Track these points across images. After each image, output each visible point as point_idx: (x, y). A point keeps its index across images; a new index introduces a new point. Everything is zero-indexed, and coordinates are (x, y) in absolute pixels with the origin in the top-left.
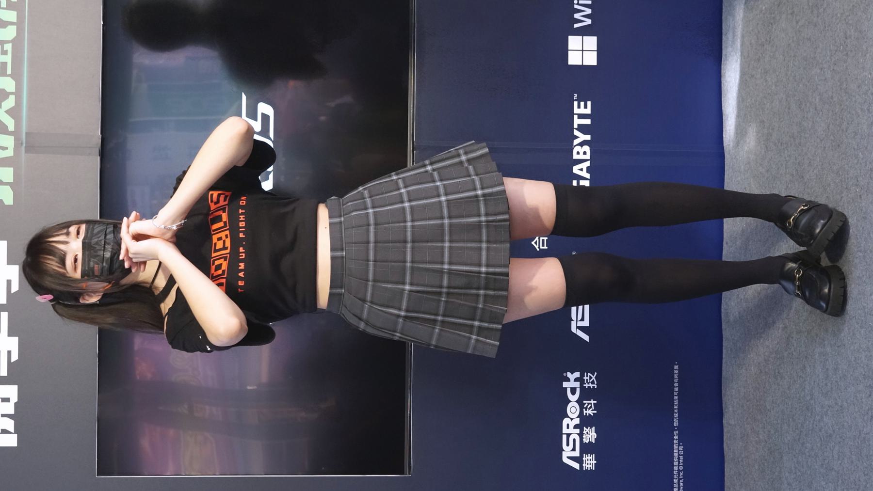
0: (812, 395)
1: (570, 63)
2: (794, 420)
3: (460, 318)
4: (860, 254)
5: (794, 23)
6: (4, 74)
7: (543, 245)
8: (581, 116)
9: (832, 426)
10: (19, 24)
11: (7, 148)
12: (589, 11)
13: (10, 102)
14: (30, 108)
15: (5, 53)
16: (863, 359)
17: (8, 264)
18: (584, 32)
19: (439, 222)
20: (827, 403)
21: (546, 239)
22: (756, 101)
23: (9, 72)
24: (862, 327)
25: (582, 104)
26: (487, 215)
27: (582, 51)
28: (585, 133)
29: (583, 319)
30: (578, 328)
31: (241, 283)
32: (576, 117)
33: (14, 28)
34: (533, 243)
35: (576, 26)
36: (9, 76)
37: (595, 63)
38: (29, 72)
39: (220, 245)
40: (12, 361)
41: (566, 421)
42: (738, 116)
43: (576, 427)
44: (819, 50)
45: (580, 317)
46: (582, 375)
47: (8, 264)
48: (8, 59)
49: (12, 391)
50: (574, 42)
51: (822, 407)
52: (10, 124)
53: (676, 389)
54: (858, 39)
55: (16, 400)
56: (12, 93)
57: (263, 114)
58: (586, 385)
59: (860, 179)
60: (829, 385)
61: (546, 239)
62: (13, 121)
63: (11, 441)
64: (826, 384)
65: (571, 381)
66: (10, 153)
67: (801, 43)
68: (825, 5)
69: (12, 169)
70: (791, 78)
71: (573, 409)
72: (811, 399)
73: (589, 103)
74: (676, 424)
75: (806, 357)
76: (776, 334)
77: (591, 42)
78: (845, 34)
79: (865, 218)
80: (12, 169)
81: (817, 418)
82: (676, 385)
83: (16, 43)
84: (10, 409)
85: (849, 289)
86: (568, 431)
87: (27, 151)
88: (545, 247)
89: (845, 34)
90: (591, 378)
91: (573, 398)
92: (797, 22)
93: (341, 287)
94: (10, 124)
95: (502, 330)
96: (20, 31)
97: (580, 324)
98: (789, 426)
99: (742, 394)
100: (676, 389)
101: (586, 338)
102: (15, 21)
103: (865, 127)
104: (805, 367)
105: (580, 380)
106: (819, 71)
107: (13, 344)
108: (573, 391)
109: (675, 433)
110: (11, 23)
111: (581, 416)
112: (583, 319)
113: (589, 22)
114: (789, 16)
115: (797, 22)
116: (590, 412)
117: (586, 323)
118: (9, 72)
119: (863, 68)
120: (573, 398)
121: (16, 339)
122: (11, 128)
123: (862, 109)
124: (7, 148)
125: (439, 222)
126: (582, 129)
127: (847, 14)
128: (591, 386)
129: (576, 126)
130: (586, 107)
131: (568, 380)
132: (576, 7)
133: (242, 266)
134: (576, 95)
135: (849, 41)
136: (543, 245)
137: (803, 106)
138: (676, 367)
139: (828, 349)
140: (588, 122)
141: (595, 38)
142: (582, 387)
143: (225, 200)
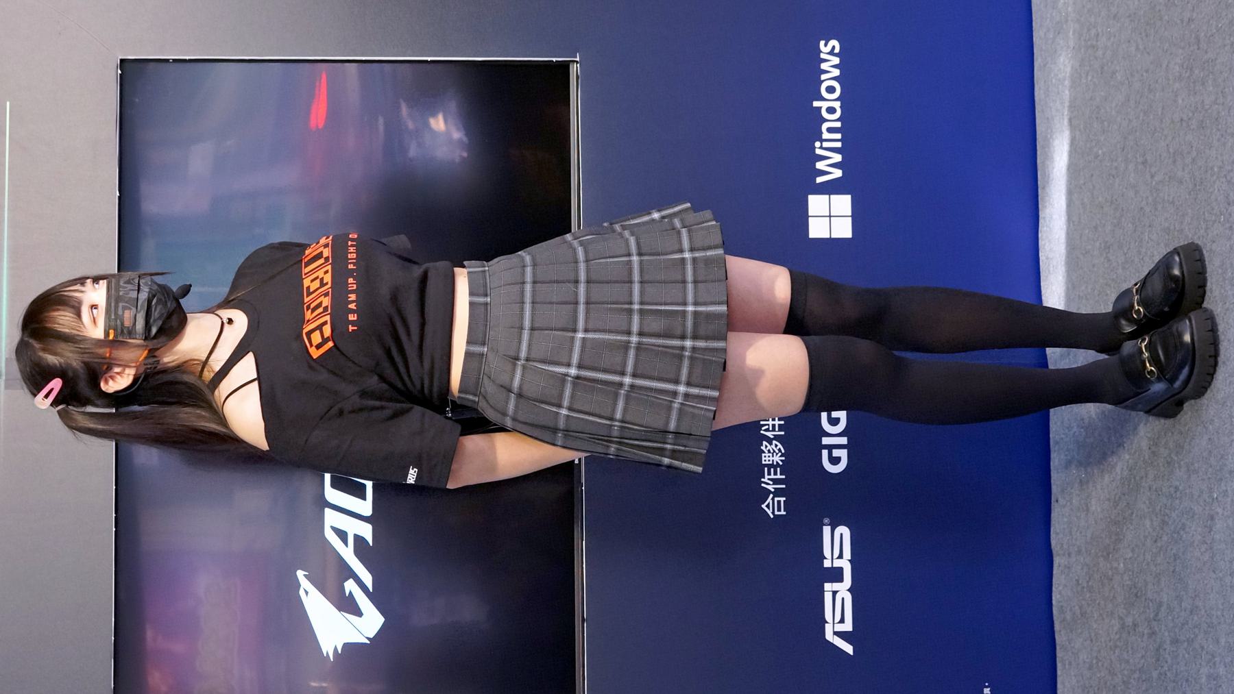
1: (811, 236)
5: (1148, 176)
7: (779, 510)
12: (838, 158)
18: (831, 188)
19: (625, 338)
21: (783, 499)
26: (692, 250)
29: (842, 621)
30: (836, 633)
31: (352, 317)
35: (819, 180)
39: (317, 284)
44: (1188, 219)
50: (816, 203)
57: (364, 498)
67: (1160, 207)
68: (1194, 154)
75: (1187, 681)
76: (1121, 463)
77: (843, 203)
78: (1227, 197)
85: (1221, 328)
92: (1152, 177)
101: (848, 649)
112: (842, 621)
113: (838, 173)
114: (1140, 167)
115: (1152, 177)
117: (848, 626)
125: (625, 338)
126: (836, 575)
132: (818, 152)
133: (353, 297)
136: (779, 510)
139: (1221, 670)
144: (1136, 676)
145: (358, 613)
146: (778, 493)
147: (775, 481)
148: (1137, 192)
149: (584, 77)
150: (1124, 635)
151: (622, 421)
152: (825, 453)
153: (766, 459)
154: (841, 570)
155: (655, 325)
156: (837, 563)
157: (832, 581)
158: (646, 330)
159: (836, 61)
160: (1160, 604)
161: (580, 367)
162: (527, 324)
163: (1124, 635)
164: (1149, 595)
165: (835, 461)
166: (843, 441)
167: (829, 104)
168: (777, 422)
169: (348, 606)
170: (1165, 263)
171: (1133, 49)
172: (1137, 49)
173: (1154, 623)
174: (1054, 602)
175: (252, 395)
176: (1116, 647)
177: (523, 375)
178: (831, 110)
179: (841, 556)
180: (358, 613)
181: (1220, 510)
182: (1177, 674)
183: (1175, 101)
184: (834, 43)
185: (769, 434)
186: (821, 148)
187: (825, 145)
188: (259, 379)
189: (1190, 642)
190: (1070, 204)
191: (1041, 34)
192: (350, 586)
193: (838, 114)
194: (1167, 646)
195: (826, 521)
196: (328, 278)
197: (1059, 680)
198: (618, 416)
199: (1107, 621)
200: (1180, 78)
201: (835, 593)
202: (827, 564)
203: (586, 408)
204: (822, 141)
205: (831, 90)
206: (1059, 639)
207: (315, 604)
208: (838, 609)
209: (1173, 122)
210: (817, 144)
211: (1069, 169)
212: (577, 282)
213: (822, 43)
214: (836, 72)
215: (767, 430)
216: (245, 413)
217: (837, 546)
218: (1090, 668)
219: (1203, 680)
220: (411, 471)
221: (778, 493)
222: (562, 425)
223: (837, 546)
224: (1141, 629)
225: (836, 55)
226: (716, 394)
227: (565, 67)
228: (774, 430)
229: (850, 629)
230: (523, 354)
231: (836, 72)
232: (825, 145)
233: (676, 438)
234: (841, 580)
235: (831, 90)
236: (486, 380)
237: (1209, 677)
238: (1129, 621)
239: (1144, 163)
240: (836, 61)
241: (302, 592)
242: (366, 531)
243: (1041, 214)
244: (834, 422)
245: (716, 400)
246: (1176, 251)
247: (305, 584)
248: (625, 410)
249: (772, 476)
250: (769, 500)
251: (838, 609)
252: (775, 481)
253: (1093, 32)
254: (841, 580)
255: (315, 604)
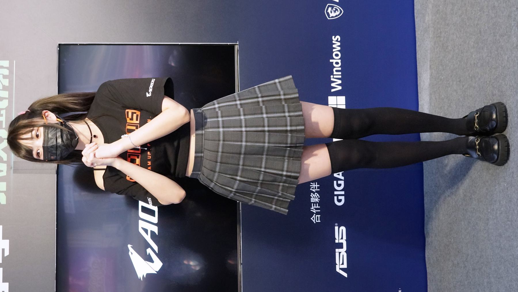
4: (509, 223)
5: (461, 87)
10: (10, 99)
11: (2, 171)
12: (340, 82)
15: (2, 115)
16: (514, 286)
18: (337, 94)
21: (319, 216)
24: (512, 267)
29: (343, 264)
30: (340, 269)
35: (333, 90)
36: (4, 129)
40: (5, 255)
45: (341, 263)
57: (154, 216)
59: (506, 178)
63: (4, 202)
66: (4, 174)
68: (479, 76)
69: (5, 183)
75: (479, 285)
80: (5, 183)
87: (14, 173)
88: (319, 221)
92: (463, 86)
93: (199, 171)
95: (297, 187)
96: (10, 102)
97: (342, 267)
101: (345, 275)
107: (6, 244)
110: (5, 98)
112: (343, 264)
113: (340, 88)
114: (458, 83)
115: (463, 86)
117: (345, 266)
121: (8, 284)
122: (5, 159)
124: (2, 171)
126: (340, 246)
127: (493, 81)
132: (332, 79)
143: (137, 120)
145: (152, 261)
146: (317, 213)
147: (316, 209)
149: (240, 50)
152: (336, 198)
153: (312, 200)
154: (342, 244)
156: (341, 241)
159: (339, 44)
160: (468, 255)
165: (339, 201)
166: (343, 193)
167: (336, 61)
168: (317, 186)
169: (149, 259)
171: (455, 37)
172: (457, 37)
174: (426, 256)
178: (337, 63)
179: (342, 238)
180: (152, 261)
181: (491, 216)
184: (338, 37)
185: (314, 190)
187: (335, 77)
191: (419, 33)
192: (149, 251)
195: (336, 224)
201: (340, 253)
202: (337, 241)
204: (333, 75)
205: (337, 55)
206: (429, 270)
207: (135, 258)
208: (341, 260)
210: (332, 76)
213: (333, 37)
214: (339, 48)
215: (313, 189)
217: (341, 234)
221: (317, 213)
223: (341, 234)
225: (339, 42)
226: (303, 127)
227: (233, 47)
228: (315, 189)
231: (339, 48)
232: (335, 77)
234: (342, 248)
235: (337, 55)
238: (456, 262)
241: (130, 254)
242: (155, 229)
244: (339, 185)
249: (315, 207)
250: (314, 216)
251: (341, 260)
252: (316, 209)
253: (439, 31)
254: (342, 248)
255: (135, 258)
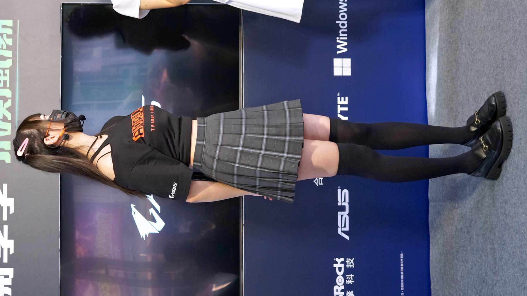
0: (486, 273)
1: (335, 75)
2: (475, 288)
3: (276, 151)
4: (515, 190)
6: (5, 87)
8: (342, 106)
9: (500, 292)
10: (14, 58)
11: (7, 130)
12: (346, 44)
13: (9, 103)
14: (20, 106)
15: (5, 75)
16: (518, 252)
17: (8, 197)
18: (343, 56)
20: (496, 278)
22: (447, 96)
23: (8, 86)
24: (517, 233)
25: (343, 98)
27: (342, 67)
28: (344, 116)
29: (345, 227)
30: (342, 231)
32: (339, 106)
33: (11, 60)
34: (314, 181)
35: (338, 52)
37: (350, 74)
38: (20, 86)
40: (10, 254)
41: (336, 287)
42: (437, 105)
43: (342, 291)
44: (486, 67)
45: (343, 225)
46: (345, 260)
47: (8, 197)
48: (7, 78)
49: (10, 272)
50: (337, 62)
51: (493, 281)
52: (9, 116)
53: (402, 268)
54: (510, 60)
55: (13, 277)
56: (9, 98)
58: (348, 266)
60: (497, 267)
61: (322, 179)
62: (10, 114)
64: (495, 267)
65: (339, 264)
67: (475, 62)
70: (469, 83)
71: (340, 280)
72: (486, 276)
73: (347, 98)
74: (402, 289)
77: (347, 62)
78: (503, 57)
79: (517, 168)
81: (490, 287)
82: (402, 265)
83: (12, 69)
84: (9, 282)
86: (337, 294)
88: (322, 184)
89: (503, 57)
90: (350, 261)
91: (340, 274)
92: (472, 50)
94: (9, 116)
96: (14, 62)
97: (344, 229)
98: (472, 291)
99: (443, 271)
100: (402, 268)
101: (347, 238)
102: (11, 56)
103: (516, 113)
104: (481, 256)
105: (344, 263)
106: (486, 79)
108: (340, 269)
109: (402, 289)
110: (9, 58)
111: (345, 284)
112: (345, 227)
113: (345, 50)
114: (467, 46)
115: (472, 50)
116: (350, 282)
117: (347, 229)
118: (8, 86)
119: (514, 78)
120: (340, 274)
122: (9, 118)
123: (514, 103)
124: (7, 130)
126: (343, 208)
127: (504, 45)
128: (351, 266)
129: (339, 112)
130: (345, 100)
131: (337, 263)
132: (338, 41)
133: (153, 120)
134: (339, 94)
135: (504, 61)
137: (477, 100)
138: (402, 255)
139: (496, 246)
140: (346, 109)
141: (350, 60)
142: (345, 267)
144: (462, 248)
145: (155, 221)
148: (466, 56)
150: (457, 233)
151: (261, 168)
154: (345, 206)
155: (274, 131)
156: (343, 204)
157: (341, 211)
158: (270, 133)
159: (346, 5)
161: (243, 147)
162: (221, 132)
163: (457, 233)
164: (468, 217)
170: (488, 101)
173: (469, 228)
175: (109, 157)
176: (454, 237)
177: (220, 151)
178: (343, 25)
179: (345, 201)
180: (155, 221)
182: (478, 248)
183: (482, 19)
186: (339, 40)
187: (341, 38)
188: (112, 152)
189: (484, 235)
190: (439, 62)
192: (152, 211)
193: (346, 26)
194: (474, 237)
195: (339, 187)
196: (143, 116)
197: (431, 251)
198: (259, 165)
199: (450, 227)
200: (484, 10)
201: (342, 216)
202: (339, 204)
203: (246, 163)
204: (339, 37)
205: (343, 16)
209: (481, 27)
210: (338, 38)
211: (438, 48)
212: (242, 118)
214: (346, 10)
216: (106, 165)
218: (443, 246)
219: (489, 250)
220: (174, 185)
222: (236, 172)
224: (464, 230)
225: (345, 3)
226: (300, 157)
229: (348, 230)
230: (220, 143)
231: (346, 10)
232: (341, 38)
233: (283, 176)
234: (344, 210)
235: (343, 16)
236: (205, 155)
237: (491, 249)
238: (459, 227)
239: (469, 44)
240: (346, 5)
241: (133, 213)
243: (427, 66)
245: (300, 159)
246: (493, 95)
247: (134, 209)
248: (262, 163)
254: (344, 210)
